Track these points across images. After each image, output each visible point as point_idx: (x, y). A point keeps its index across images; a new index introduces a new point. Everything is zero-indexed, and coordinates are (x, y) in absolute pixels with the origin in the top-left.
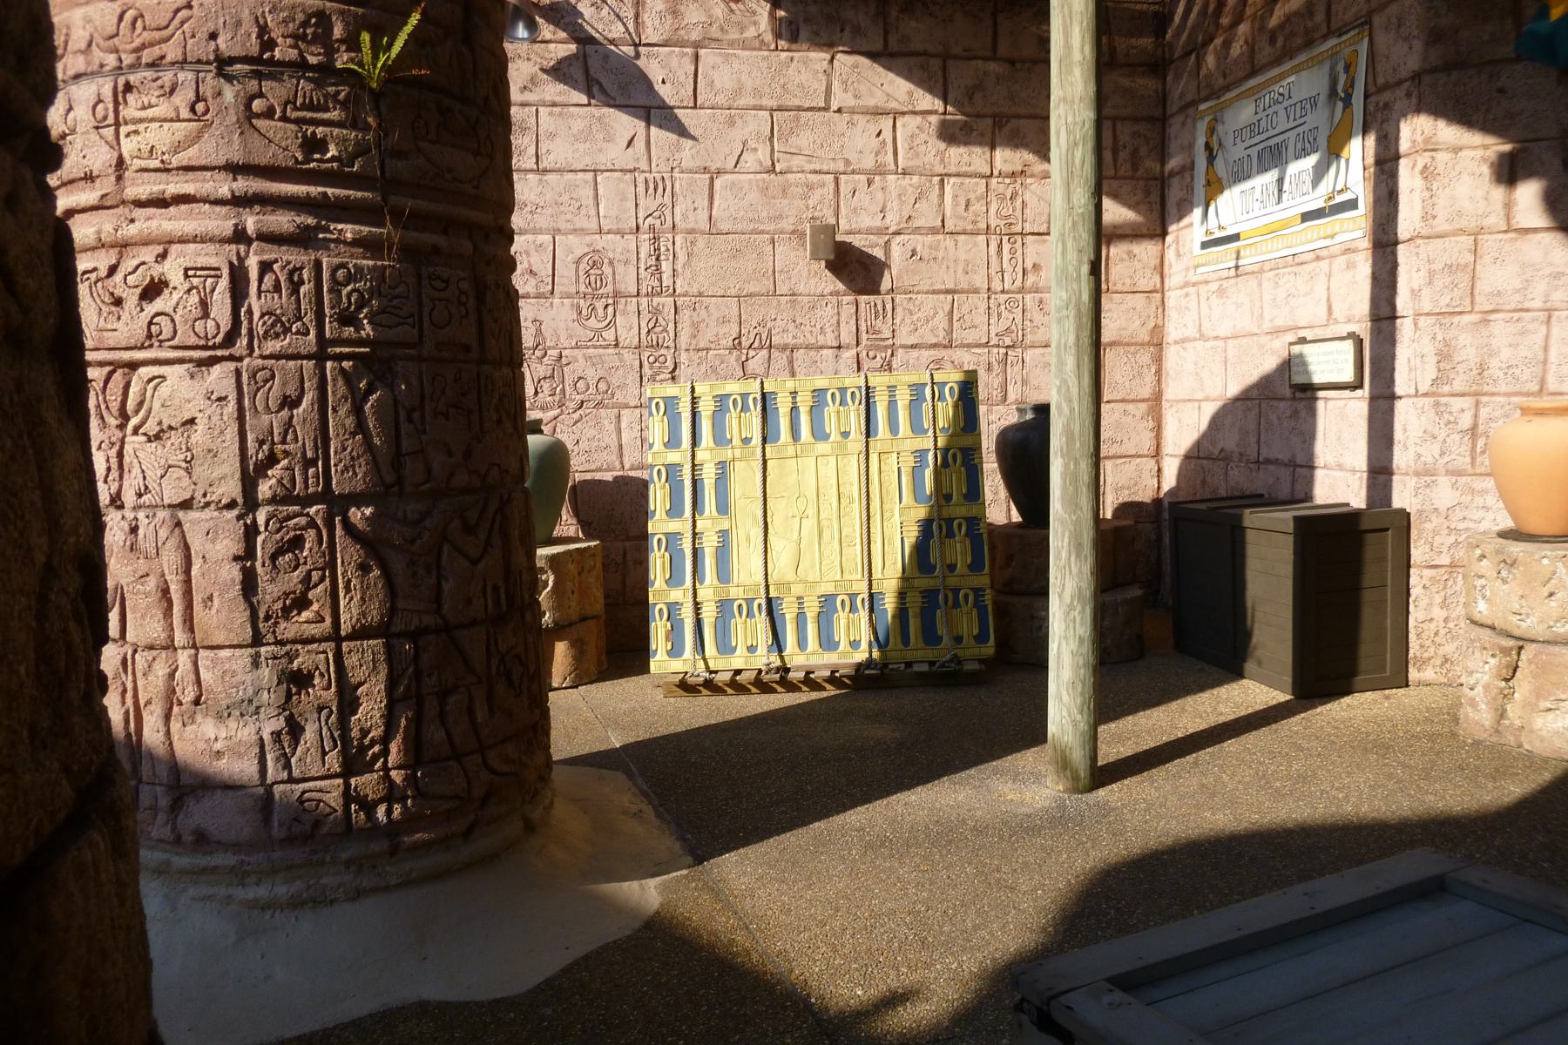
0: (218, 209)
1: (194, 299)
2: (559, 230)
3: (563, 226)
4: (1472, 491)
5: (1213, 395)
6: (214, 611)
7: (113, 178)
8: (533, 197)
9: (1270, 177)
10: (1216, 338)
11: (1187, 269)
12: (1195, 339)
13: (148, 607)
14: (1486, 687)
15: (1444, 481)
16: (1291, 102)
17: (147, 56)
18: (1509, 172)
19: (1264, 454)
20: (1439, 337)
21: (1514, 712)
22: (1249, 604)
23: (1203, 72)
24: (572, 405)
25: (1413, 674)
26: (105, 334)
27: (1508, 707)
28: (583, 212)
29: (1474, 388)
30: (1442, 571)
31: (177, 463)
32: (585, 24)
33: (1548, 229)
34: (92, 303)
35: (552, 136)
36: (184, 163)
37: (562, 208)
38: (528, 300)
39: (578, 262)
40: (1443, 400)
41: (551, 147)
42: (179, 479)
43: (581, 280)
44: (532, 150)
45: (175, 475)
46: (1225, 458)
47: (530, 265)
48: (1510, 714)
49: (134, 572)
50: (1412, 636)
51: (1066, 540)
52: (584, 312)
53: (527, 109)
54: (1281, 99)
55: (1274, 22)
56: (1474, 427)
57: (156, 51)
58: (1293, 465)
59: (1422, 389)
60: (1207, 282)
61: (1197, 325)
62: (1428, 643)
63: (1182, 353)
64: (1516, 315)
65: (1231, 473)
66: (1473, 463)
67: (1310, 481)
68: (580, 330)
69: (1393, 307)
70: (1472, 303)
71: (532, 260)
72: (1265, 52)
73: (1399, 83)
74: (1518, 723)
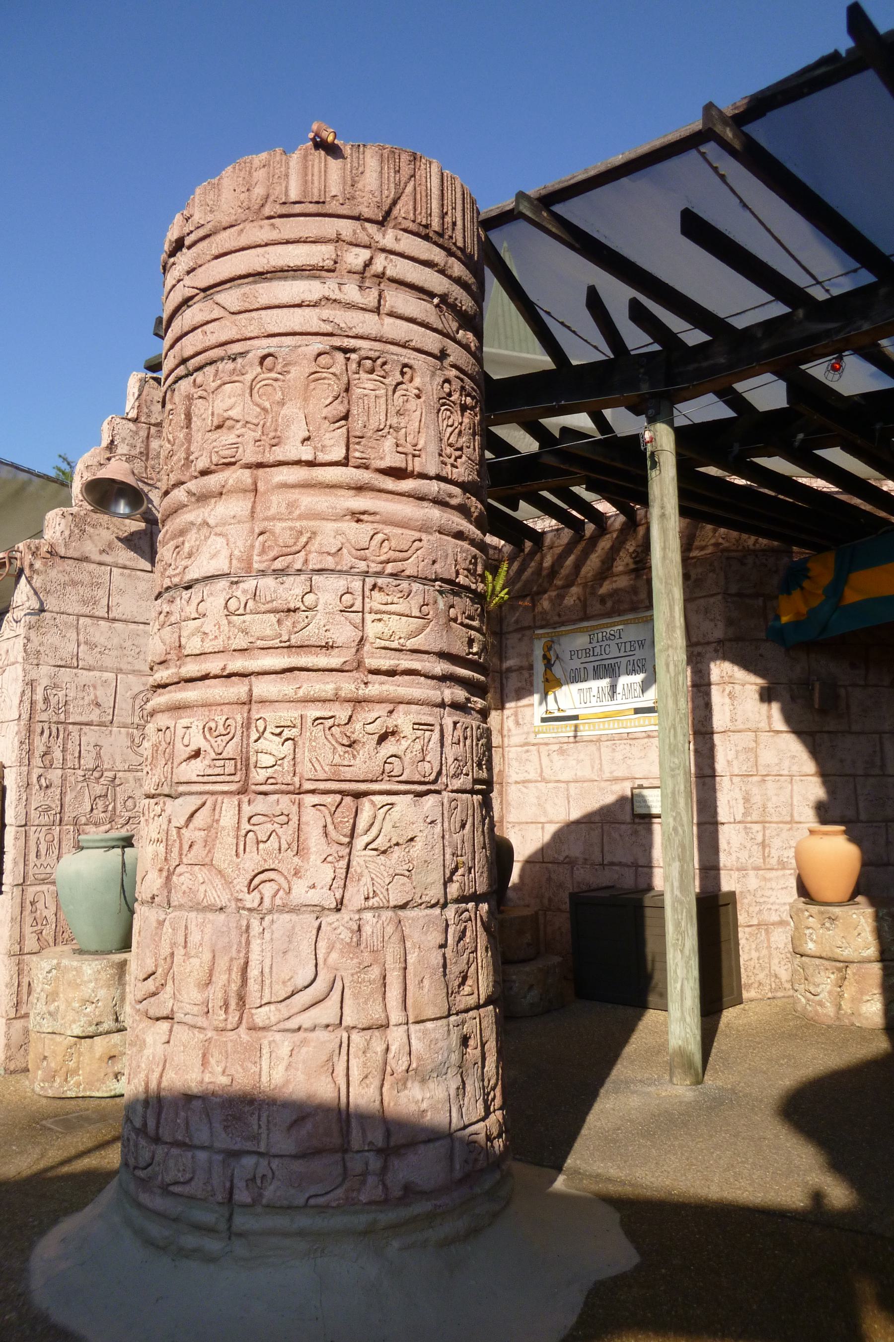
0: (429, 681)
1: (418, 746)
2: (121, 670)
3: (124, 666)
4: (765, 879)
5: (556, 820)
6: (426, 990)
7: (354, 650)
8: (102, 640)
9: (605, 683)
10: (558, 781)
11: (528, 733)
12: (536, 781)
13: (372, 993)
14: (830, 993)
15: (752, 873)
16: (620, 641)
17: (390, 569)
18: (766, 696)
19: (608, 858)
20: (743, 789)
21: (846, 1006)
22: (649, 958)
23: (538, 609)
24: (122, 821)
25: (745, 995)
26: (341, 768)
27: (842, 1003)
28: (142, 656)
29: (762, 818)
30: (754, 928)
31: (403, 872)
32: (153, 509)
33: (787, 732)
34: (327, 743)
35: (122, 592)
36: (416, 647)
37: (125, 652)
38: (92, 727)
39: (134, 698)
40: (748, 825)
41: (120, 601)
42: (403, 884)
43: (136, 713)
44: (104, 602)
45: (401, 882)
46: (571, 862)
47: (96, 697)
48: (844, 1007)
49: (360, 963)
50: (742, 970)
51: (684, 914)
52: (137, 741)
53: (103, 567)
54: (612, 638)
55: (603, 591)
56: (764, 840)
57: (399, 566)
58: (636, 866)
59: (738, 818)
60: (546, 744)
61: (539, 771)
62: (750, 974)
63: (524, 790)
64: (777, 778)
65: (576, 872)
66: (764, 862)
67: (650, 876)
68: (132, 756)
69: (713, 769)
70: (757, 770)
71: (98, 693)
72: (595, 607)
73: (708, 643)
74: (849, 1011)
